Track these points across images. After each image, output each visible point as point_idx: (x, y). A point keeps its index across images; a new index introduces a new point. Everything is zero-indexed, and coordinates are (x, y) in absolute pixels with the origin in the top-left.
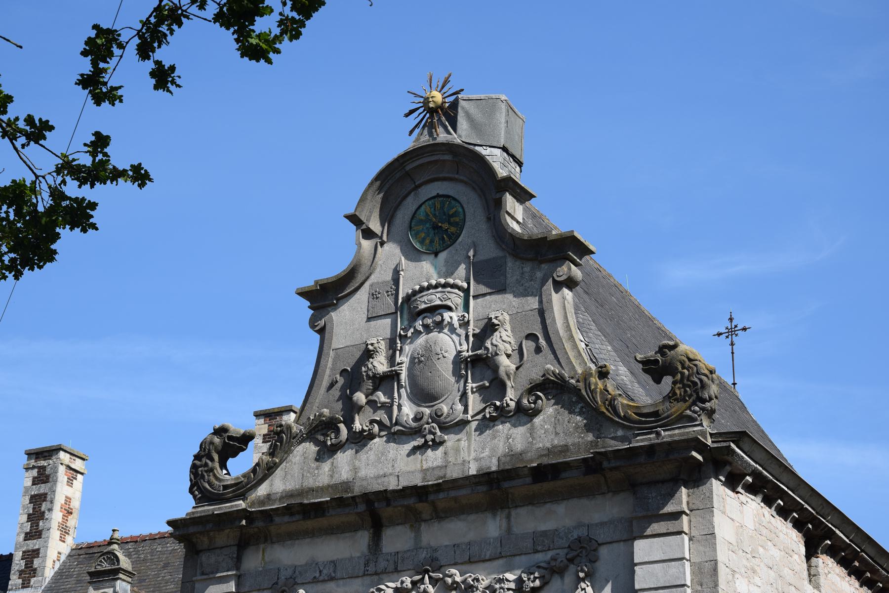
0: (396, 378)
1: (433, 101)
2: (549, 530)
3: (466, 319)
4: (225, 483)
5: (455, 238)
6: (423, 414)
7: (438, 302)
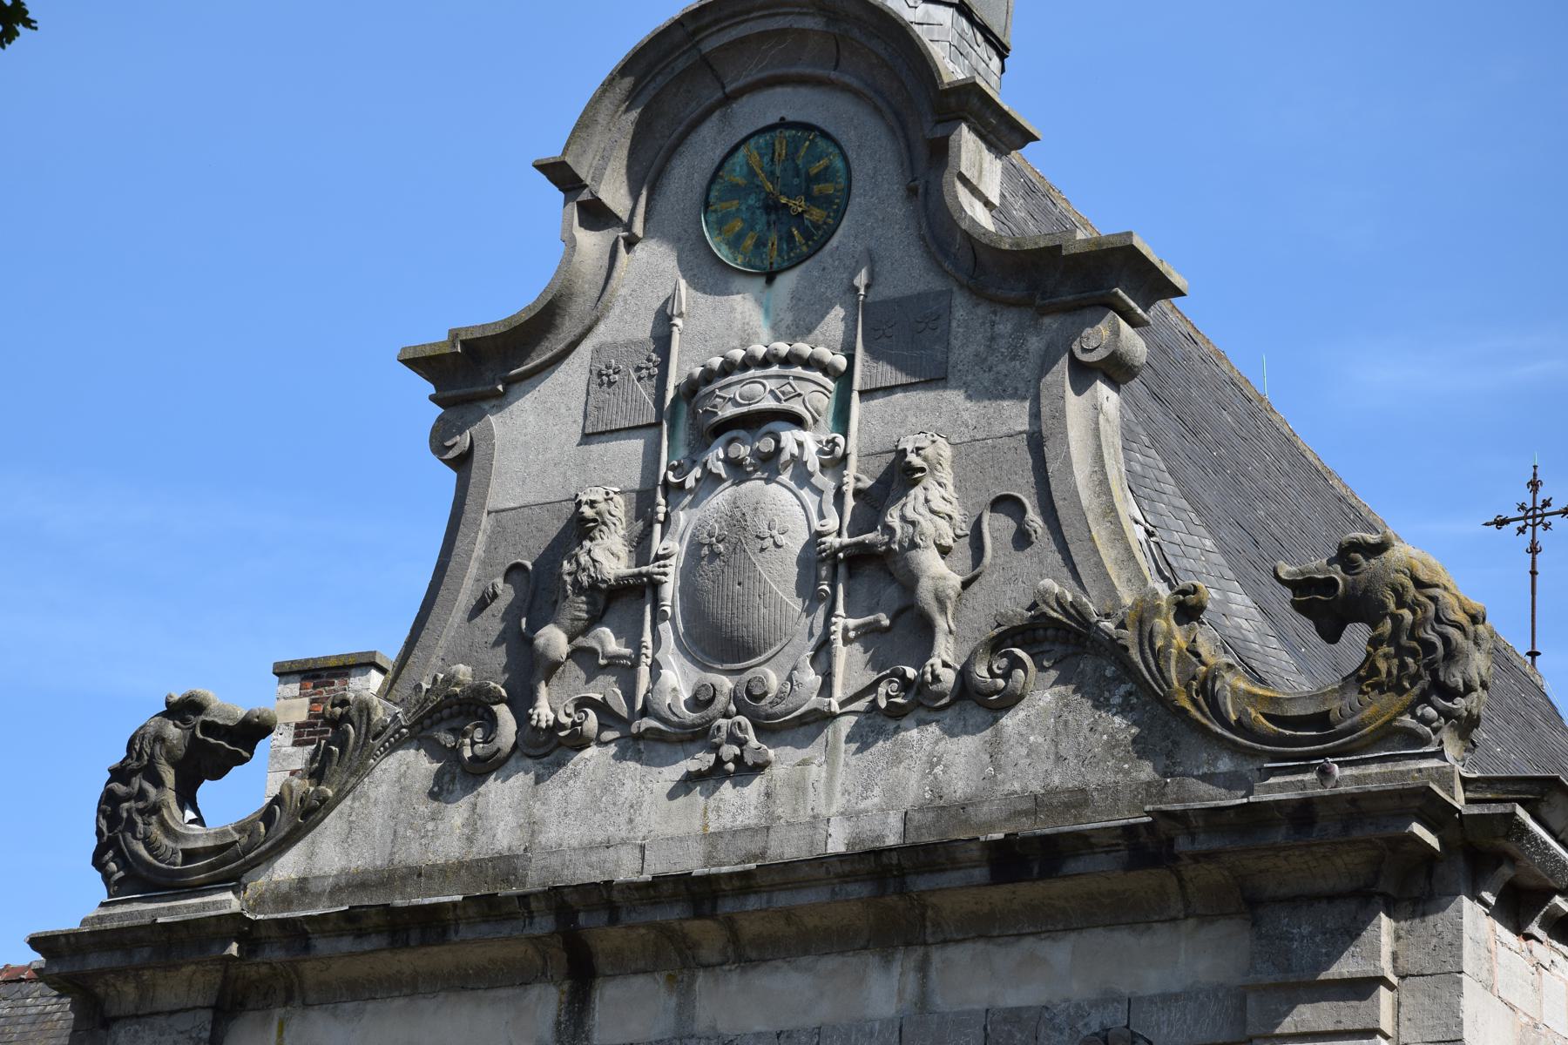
0: (649, 593)
3: (839, 451)
5: (822, 236)
6: (715, 690)
7: (769, 403)
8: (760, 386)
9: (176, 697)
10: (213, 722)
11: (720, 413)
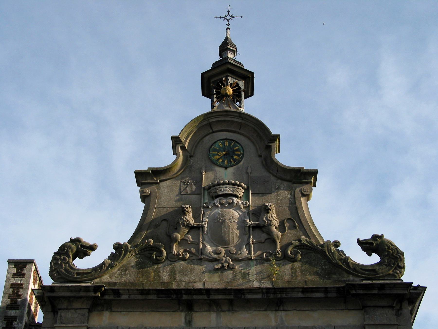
0: (201, 229)
1: (228, 91)
2: (309, 326)
3: (248, 205)
4: (78, 272)
6: (221, 250)
7: (230, 192)
8: (228, 189)
9: (73, 238)
10: (84, 245)
11: (234, 193)
